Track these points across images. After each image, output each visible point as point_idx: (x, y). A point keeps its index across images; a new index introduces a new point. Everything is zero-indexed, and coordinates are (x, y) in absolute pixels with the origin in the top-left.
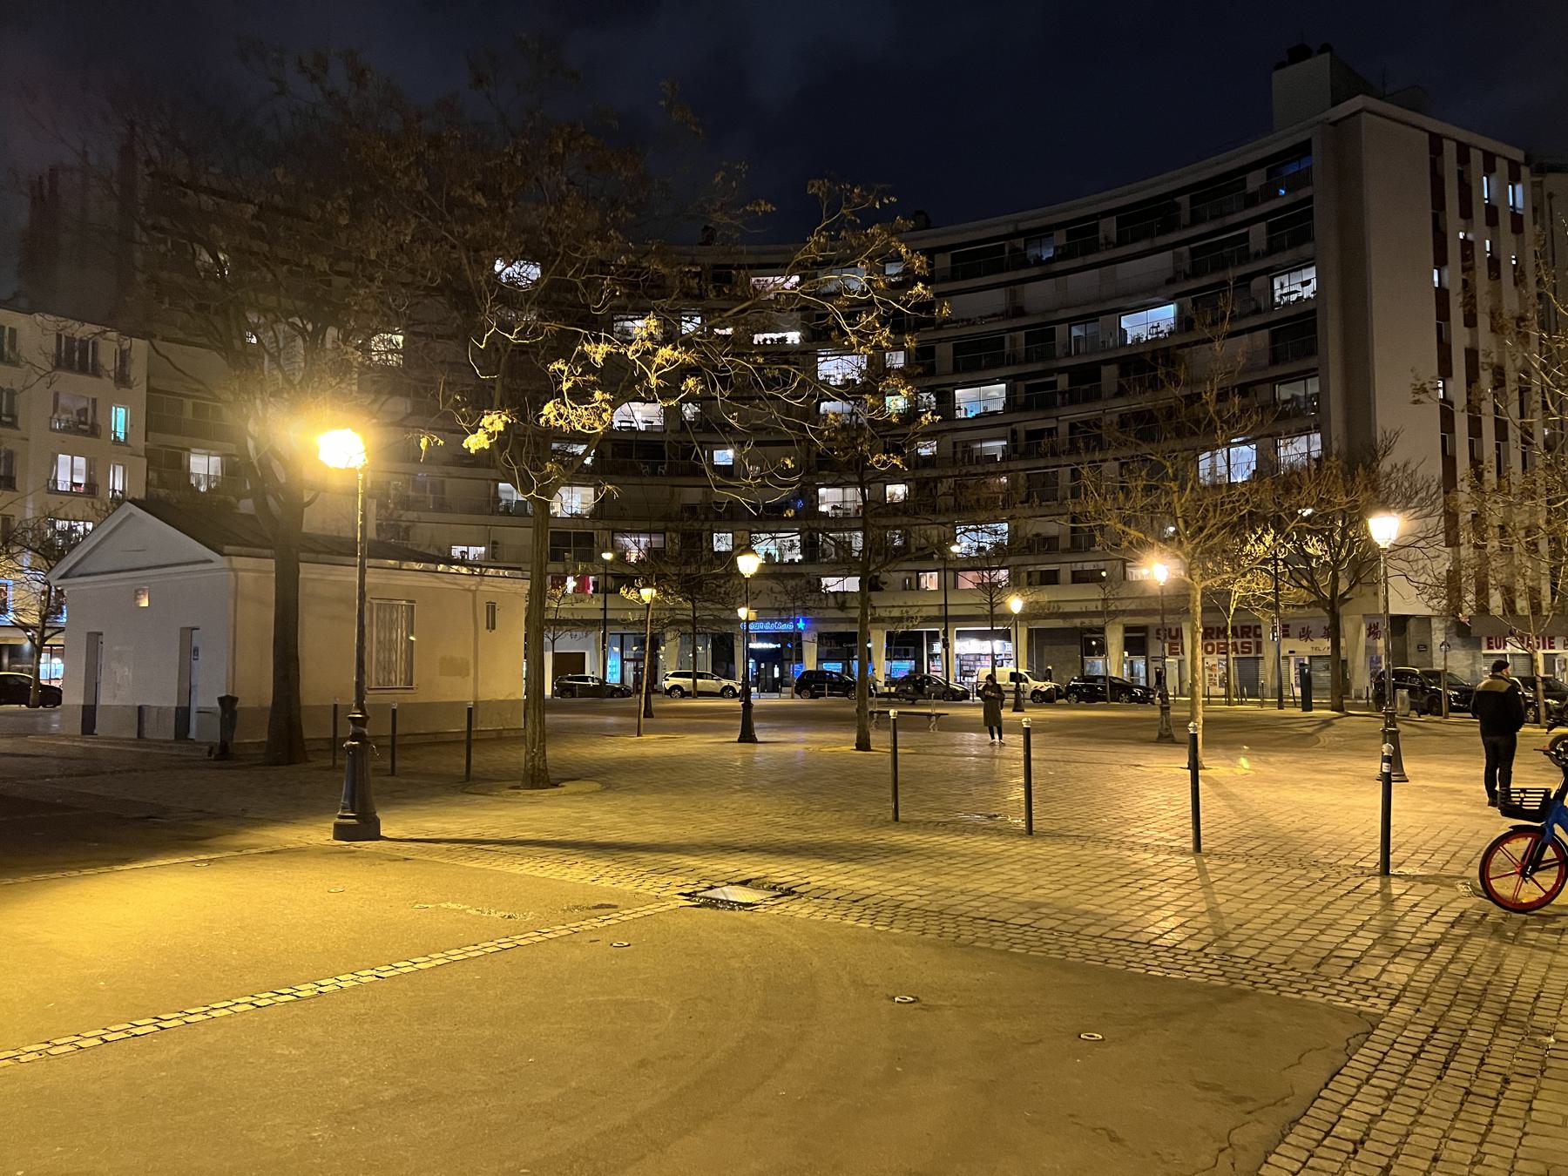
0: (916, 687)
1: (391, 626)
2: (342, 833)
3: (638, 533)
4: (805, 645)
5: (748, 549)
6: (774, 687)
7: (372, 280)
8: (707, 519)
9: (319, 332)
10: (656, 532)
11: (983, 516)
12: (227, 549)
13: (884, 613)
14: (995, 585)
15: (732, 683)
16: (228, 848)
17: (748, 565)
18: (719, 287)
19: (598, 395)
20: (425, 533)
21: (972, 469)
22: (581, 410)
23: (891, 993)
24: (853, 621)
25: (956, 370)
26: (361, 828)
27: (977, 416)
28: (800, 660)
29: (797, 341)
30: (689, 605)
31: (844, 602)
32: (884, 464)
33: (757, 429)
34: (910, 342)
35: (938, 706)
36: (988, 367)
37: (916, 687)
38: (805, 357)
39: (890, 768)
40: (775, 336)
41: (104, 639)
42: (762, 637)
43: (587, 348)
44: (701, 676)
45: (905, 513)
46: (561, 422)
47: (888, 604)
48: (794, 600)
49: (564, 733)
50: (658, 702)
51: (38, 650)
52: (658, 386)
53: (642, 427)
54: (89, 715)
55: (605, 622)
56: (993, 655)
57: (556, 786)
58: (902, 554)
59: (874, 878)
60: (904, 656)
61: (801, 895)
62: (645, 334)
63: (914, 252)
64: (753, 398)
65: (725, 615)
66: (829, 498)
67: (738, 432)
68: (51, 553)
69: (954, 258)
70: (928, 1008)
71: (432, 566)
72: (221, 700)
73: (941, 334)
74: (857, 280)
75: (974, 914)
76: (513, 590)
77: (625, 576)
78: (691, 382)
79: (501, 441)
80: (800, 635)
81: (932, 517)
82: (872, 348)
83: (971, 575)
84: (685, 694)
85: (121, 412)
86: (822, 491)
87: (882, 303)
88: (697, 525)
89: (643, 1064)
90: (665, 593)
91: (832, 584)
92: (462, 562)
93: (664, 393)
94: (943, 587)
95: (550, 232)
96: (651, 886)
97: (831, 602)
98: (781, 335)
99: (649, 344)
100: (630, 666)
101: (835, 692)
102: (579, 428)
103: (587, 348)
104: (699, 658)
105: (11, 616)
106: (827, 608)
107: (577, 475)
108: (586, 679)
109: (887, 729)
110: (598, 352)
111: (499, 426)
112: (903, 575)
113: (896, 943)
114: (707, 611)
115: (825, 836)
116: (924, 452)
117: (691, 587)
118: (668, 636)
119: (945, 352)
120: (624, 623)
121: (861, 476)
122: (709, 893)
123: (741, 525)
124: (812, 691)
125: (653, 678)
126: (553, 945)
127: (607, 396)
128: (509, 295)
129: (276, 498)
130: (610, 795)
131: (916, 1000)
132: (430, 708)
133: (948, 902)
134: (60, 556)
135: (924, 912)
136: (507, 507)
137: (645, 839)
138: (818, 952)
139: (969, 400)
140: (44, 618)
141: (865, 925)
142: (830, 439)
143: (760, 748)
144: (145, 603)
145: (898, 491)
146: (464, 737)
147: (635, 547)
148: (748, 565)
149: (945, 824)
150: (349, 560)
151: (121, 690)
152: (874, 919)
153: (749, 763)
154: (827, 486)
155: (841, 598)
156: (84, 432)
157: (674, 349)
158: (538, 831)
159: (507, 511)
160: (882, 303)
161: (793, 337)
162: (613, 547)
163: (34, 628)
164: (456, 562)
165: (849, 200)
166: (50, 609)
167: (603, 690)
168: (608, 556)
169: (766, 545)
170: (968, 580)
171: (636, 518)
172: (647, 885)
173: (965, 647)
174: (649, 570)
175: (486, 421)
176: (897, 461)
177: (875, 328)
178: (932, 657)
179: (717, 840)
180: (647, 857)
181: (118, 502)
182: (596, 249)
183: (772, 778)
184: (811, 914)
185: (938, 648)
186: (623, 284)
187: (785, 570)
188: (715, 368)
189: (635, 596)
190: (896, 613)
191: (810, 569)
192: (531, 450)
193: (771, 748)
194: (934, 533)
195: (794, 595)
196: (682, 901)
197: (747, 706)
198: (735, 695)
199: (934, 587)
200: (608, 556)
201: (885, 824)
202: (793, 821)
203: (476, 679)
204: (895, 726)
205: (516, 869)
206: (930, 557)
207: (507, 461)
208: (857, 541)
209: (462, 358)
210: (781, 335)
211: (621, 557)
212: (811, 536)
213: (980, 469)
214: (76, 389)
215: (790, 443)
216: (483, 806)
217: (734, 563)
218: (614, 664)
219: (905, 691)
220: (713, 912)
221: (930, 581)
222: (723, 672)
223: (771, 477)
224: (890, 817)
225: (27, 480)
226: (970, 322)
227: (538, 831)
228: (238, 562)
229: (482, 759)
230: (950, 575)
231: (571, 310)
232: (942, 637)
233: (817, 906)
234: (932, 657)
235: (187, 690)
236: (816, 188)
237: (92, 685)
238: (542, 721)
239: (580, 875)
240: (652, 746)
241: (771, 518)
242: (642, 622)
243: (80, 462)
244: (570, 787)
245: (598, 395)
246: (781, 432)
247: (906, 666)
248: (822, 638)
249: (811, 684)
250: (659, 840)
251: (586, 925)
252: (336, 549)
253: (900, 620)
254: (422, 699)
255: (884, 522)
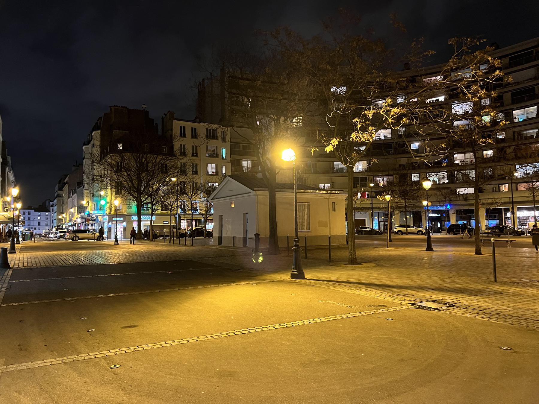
0: (500, 230)
1: (303, 210)
2: (293, 276)
3: (383, 176)
4: (450, 215)
5: (427, 179)
6: (439, 231)
7: (295, 100)
8: (409, 169)
9: (279, 119)
10: (392, 175)
11: (530, 160)
12: (255, 189)
13: (484, 201)
14: (535, 188)
15: (421, 229)
16: (264, 280)
17: (427, 185)
18: (411, 84)
19: (370, 128)
20: (310, 182)
21: (524, 142)
22: (364, 134)
23: (500, 345)
24: (472, 205)
25: (513, 103)
26: (299, 275)
27: (524, 121)
28: (449, 220)
29: (443, 100)
30: (403, 201)
31: (467, 198)
32: (485, 142)
33: (430, 134)
34: (494, 94)
35: (511, 237)
36: (528, 100)
37: (500, 230)
38: (447, 104)
39: (492, 262)
40: (434, 99)
41: (223, 217)
42: (433, 212)
43: (366, 112)
44: (409, 227)
45: (493, 161)
46: (357, 139)
47: (486, 198)
48: (445, 198)
49: (361, 246)
50: (393, 236)
51: (206, 221)
52: (392, 122)
53: (383, 138)
54: (220, 238)
55: (372, 208)
56: (535, 217)
57: (360, 264)
58: (492, 177)
59: (488, 303)
60: (494, 218)
61: (457, 307)
62: (387, 105)
63: (494, 59)
64: (429, 123)
65: (417, 204)
66: (458, 158)
67: (422, 136)
68: (208, 192)
69: (510, 59)
70: (516, 352)
71: (314, 191)
72: (255, 235)
73: (506, 90)
74: (468, 74)
75: (534, 319)
76: (341, 198)
77: (379, 192)
78: (404, 120)
79: (337, 148)
80: (448, 211)
81: (506, 162)
82: (478, 98)
83: (523, 185)
84: (403, 233)
85: (224, 150)
86: (455, 156)
87: (481, 80)
88: (405, 172)
89: (402, 360)
90: (394, 197)
91: (461, 191)
92: (324, 190)
93: (394, 125)
94: (511, 190)
95: (352, 74)
96: (397, 300)
97: (461, 198)
98: (436, 99)
99: (388, 108)
100: (382, 223)
101: (463, 231)
102: (364, 140)
103: (366, 112)
104: (408, 220)
105: (199, 211)
106: (460, 200)
107: (362, 157)
108: (366, 228)
109: (491, 246)
110: (370, 113)
111: (337, 143)
112: (492, 186)
113: (500, 327)
114: (410, 203)
115: (465, 286)
116: (500, 137)
117: (404, 194)
118: (396, 213)
119: (508, 97)
120: (379, 208)
121: (473, 148)
122: (420, 304)
123: (423, 171)
124: (454, 232)
125: (391, 228)
126: (365, 317)
127: (374, 128)
128: (338, 98)
129: (268, 172)
130: (379, 268)
131: (511, 349)
132: (316, 237)
133: (522, 313)
134: (210, 194)
135: (512, 317)
136: (337, 170)
137: (394, 284)
138: (467, 328)
139: (519, 115)
140: (207, 211)
141: (486, 319)
142: (460, 135)
143: (435, 253)
144: (233, 206)
145: (489, 153)
146: (328, 247)
147: (382, 181)
148: (427, 185)
149: (518, 283)
150: (291, 190)
151: (227, 233)
152: (489, 317)
153: (430, 258)
154: (458, 153)
155: (466, 197)
156: (214, 157)
157: (398, 108)
158: (355, 279)
159: (337, 172)
160: (481, 80)
161: (442, 98)
162: (374, 181)
163: (204, 214)
164: (322, 189)
165: (466, 44)
166: (208, 210)
167: (372, 232)
168: (372, 185)
169: (434, 177)
170: (522, 187)
171: (383, 171)
172: (397, 299)
173: (521, 214)
174: (388, 189)
175: (332, 142)
176: (490, 141)
177: (479, 90)
178: (506, 218)
179: (422, 286)
180: (396, 290)
181: (225, 177)
182: (368, 78)
183: (441, 264)
184: (463, 314)
185: (509, 214)
186: (379, 88)
187: (441, 186)
188: (413, 114)
189: (383, 199)
190: (490, 201)
191: (452, 186)
192: (347, 150)
193: (440, 253)
194: (506, 169)
195: (445, 196)
196: (410, 306)
197: (429, 237)
198: (423, 234)
199: (507, 190)
200: (372, 185)
201: (490, 282)
202: (451, 280)
203: (330, 228)
204: (494, 245)
205: (349, 291)
206: (504, 178)
207: (339, 154)
208: (473, 174)
209: (327, 123)
210: (436, 99)
211: (377, 185)
212: (451, 173)
213: (527, 142)
214: (212, 144)
215: (444, 138)
216: (335, 270)
217: (421, 184)
218: (376, 222)
219: (495, 232)
220: (423, 310)
221: (505, 188)
222: (417, 225)
223: (436, 151)
224: (493, 280)
225: (201, 172)
226: (518, 83)
227: (355, 279)
228: (258, 193)
229: (335, 254)
230: (514, 185)
231: (359, 100)
232: (511, 210)
233: (467, 309)
234: (506, 218)
235: (246, 232)
236: (451, 41)
237: (221, 231)
238: (354, 242)
239: (372, 294)
240: (393, 251)
241: (436, 167)
242: (387, 208)
243: (214, 166)
244: (365, 265)
245: (370, 128)
246: (440, 134)
247: (494, 222)
248: (458, 212)
249: (453, 229)
250: (399, 284)
251: (376, 312)
252: (286, 187)
253: (492, 204)
254: (313, 234)
255: (484, 165)
